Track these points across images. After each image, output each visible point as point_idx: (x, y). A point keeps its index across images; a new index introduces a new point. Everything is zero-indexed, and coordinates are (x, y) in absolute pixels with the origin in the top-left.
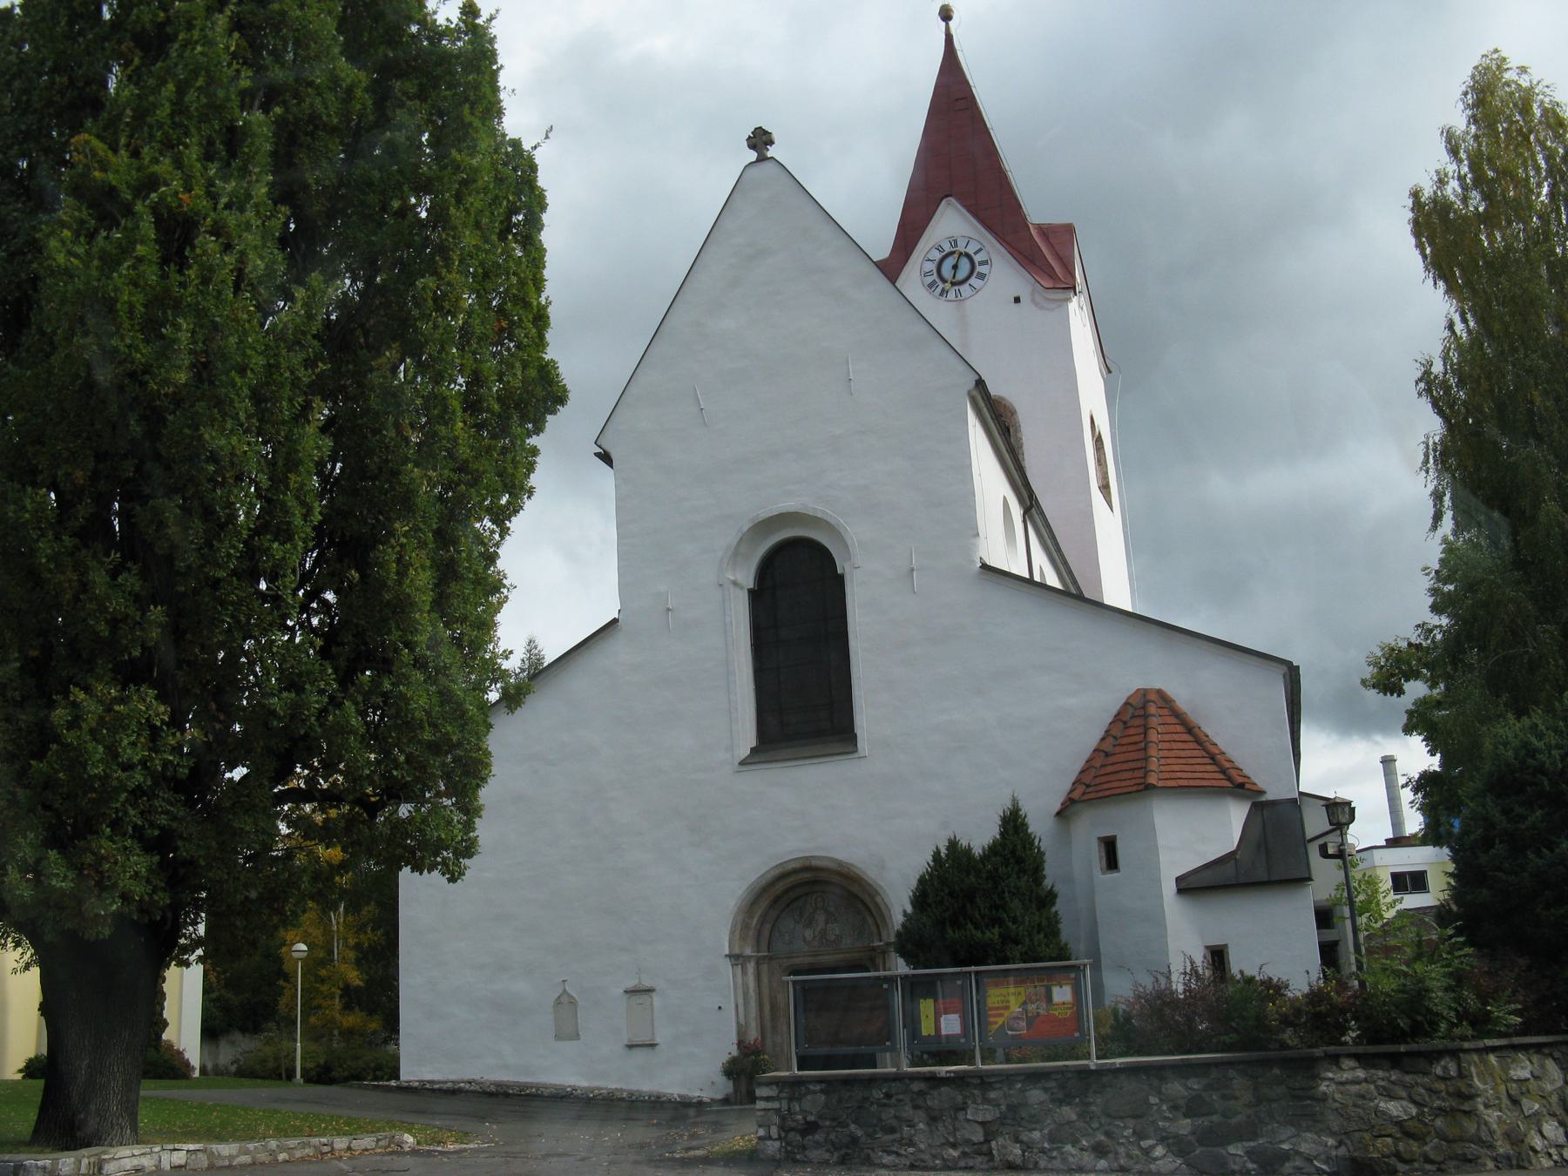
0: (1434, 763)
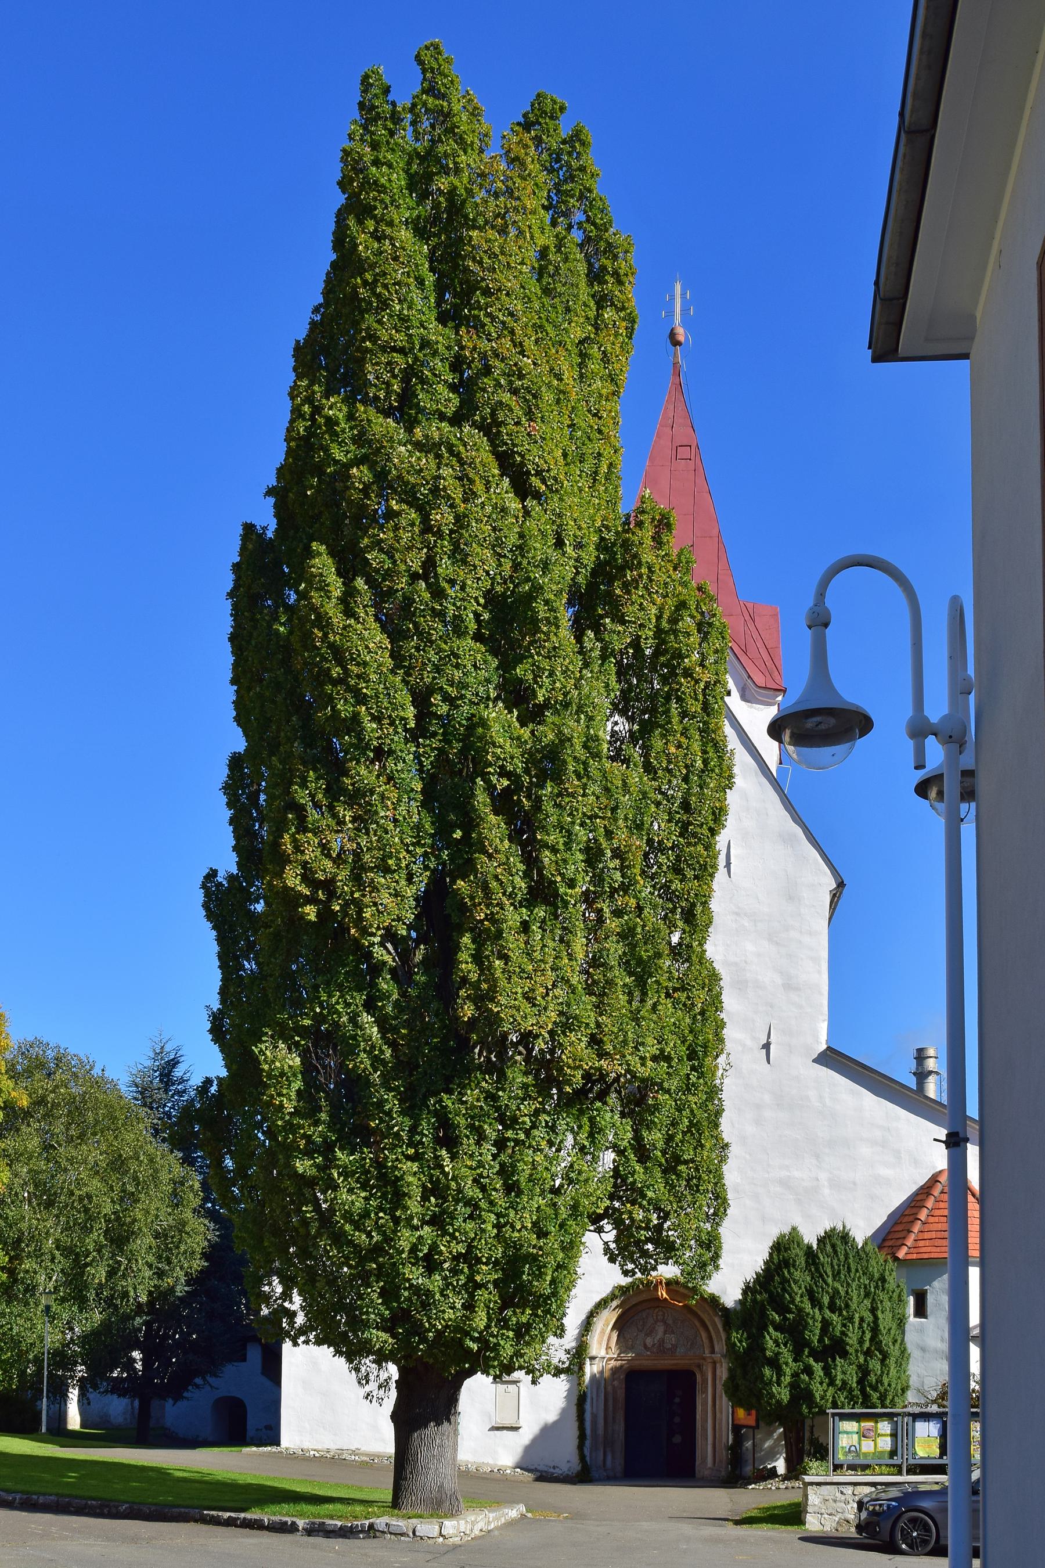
0: (235, 872)
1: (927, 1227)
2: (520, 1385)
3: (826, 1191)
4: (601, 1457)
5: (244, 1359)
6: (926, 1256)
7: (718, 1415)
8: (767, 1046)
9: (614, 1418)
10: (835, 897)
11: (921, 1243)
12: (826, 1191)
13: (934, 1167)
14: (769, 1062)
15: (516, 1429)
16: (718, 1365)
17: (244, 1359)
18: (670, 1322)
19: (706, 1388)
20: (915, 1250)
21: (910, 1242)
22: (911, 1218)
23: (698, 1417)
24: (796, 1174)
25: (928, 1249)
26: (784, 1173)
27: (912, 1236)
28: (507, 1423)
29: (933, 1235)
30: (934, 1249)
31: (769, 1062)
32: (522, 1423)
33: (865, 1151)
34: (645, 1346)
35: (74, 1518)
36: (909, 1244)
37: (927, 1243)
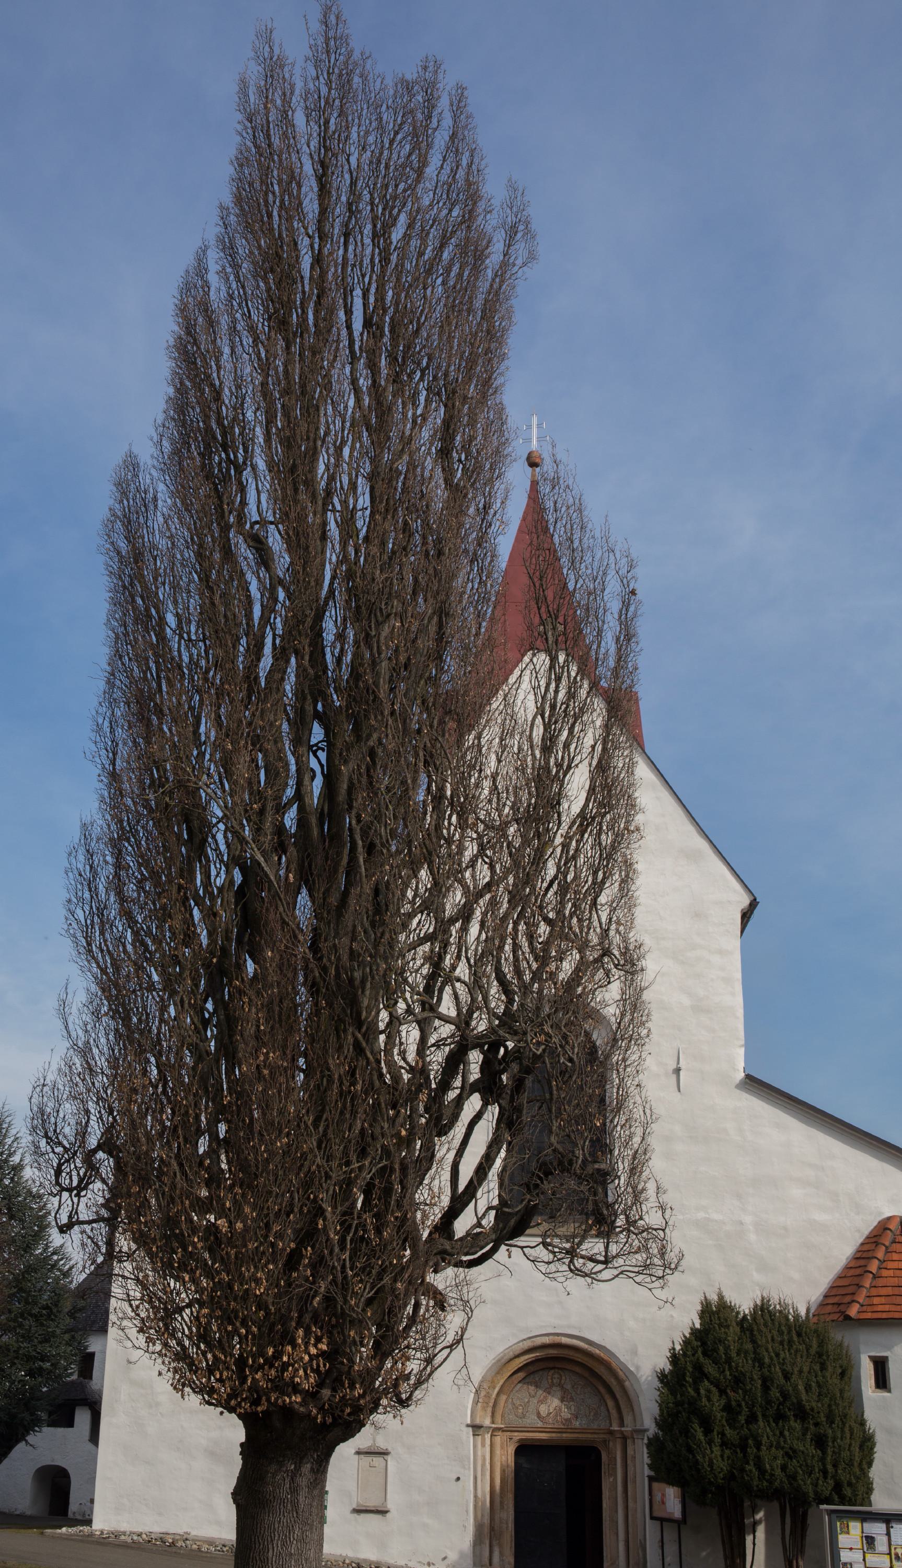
1: (880, 1282)
2: (389, 1458)
3: (753, 1237)
4: (487, 1554)
5: (71, 1424)
6: (884, 1316)
7: (631, 1504)
8: (677, 1071)
9: (502, 1503)
10: (746, 916)
11: (876, 1301)
12: (753, 1237)
13: (880, 1213)
14: (679, 1091)
15: (383, 1512)
16: (629, 1442)
17: (71, 1424)
18: (568, 1387)
19: (615, 1469)
20: (869, 1309)
21: (861, 1297)
22: (848, 1299)
23: (604, 1505)
24: (716, 1216)
25: (887, 1308)
26: (701, 1215)
27: (864, 1292)
28: (372, 1503)
29: (889, 1291)
30: (893, 1308)
31: (679, 1091)
32: (390, 1505)
33: (797, 1192)
34: (539, 1414)
35: (521, 514)
36: (861, 1301)
37: (883, 1300)
